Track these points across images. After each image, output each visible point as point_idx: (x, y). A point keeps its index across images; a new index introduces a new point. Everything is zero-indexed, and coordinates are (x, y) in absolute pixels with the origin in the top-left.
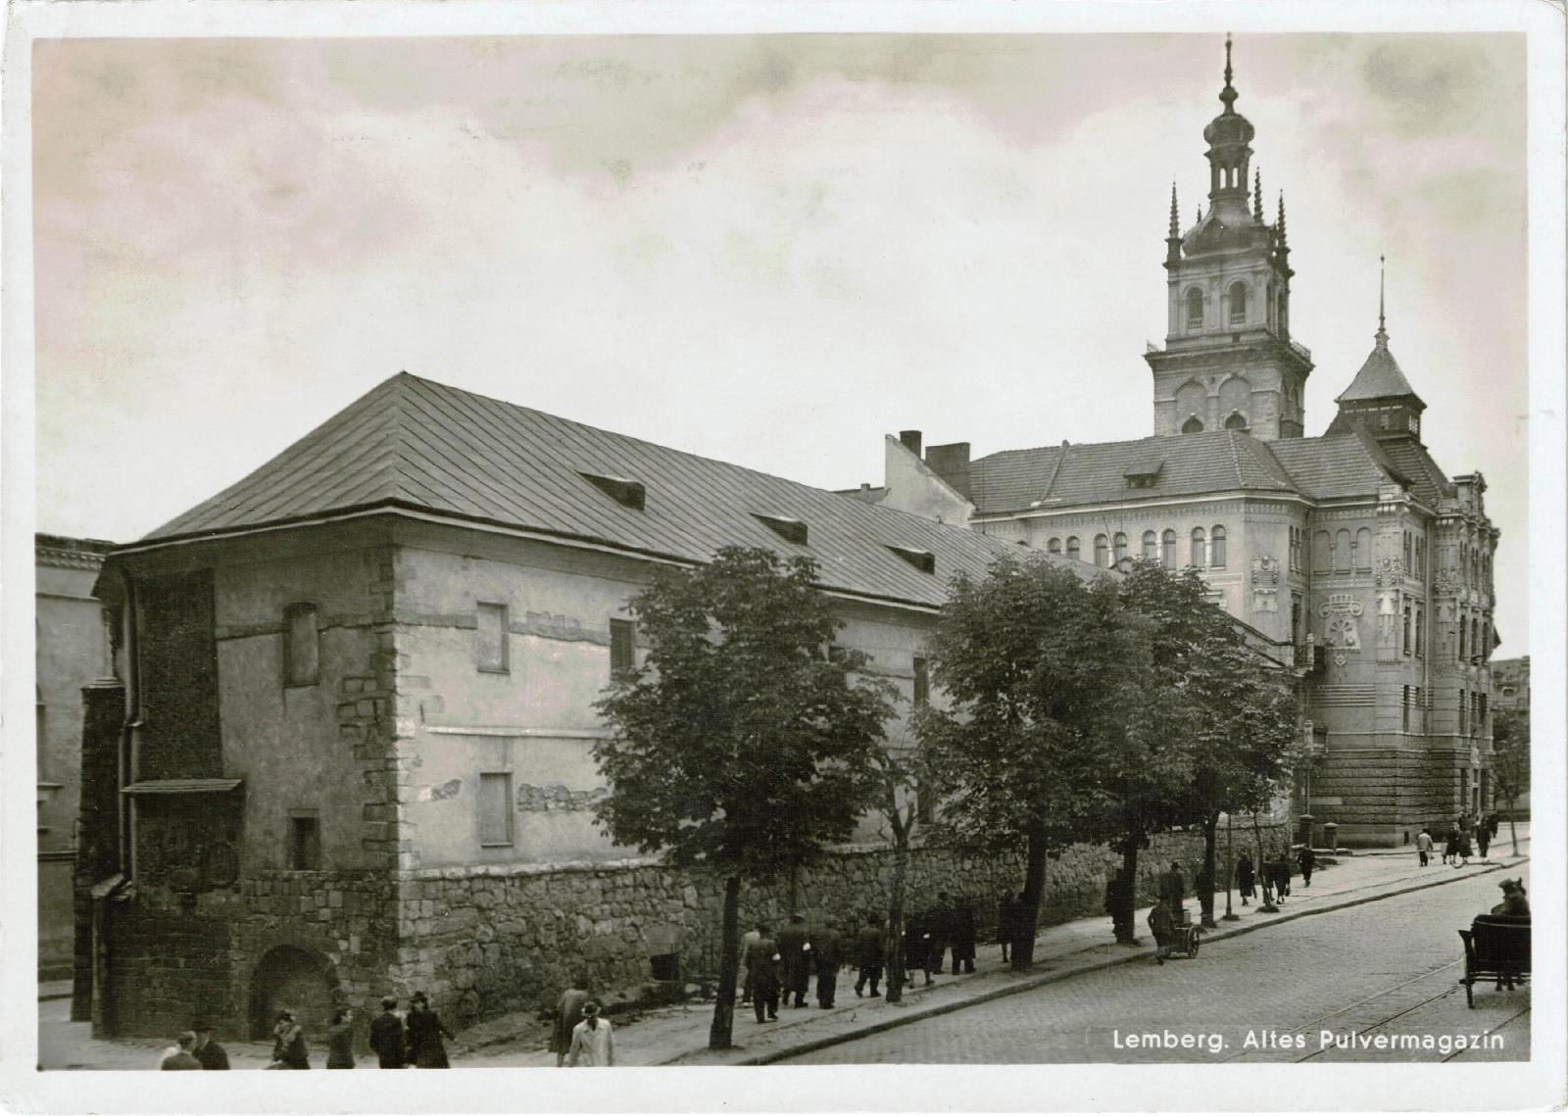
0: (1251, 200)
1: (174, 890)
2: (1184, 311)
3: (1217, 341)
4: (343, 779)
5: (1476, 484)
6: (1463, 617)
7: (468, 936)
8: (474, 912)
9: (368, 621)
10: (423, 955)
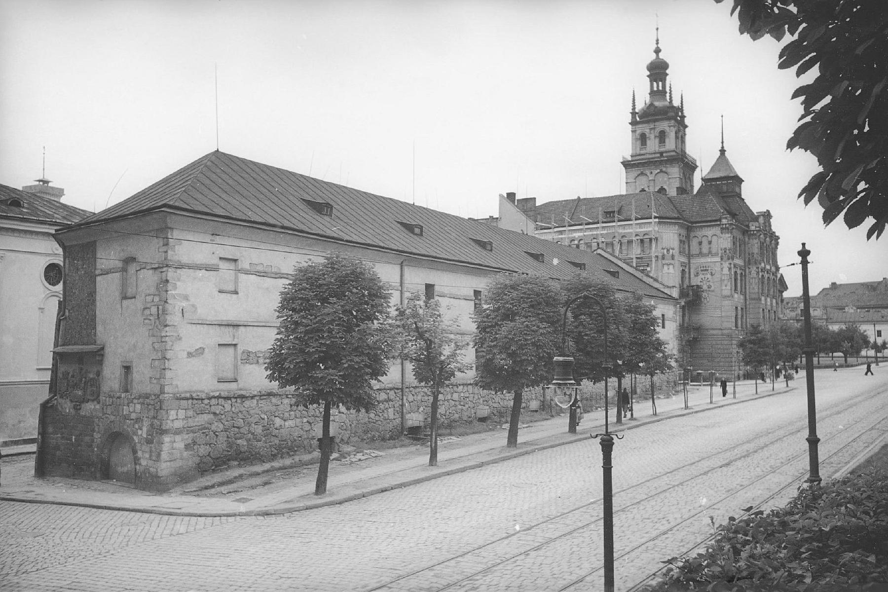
0: (668, 95)
1: (71, 401)
2: (639, 143)
3: (653, 156)
4: (143, 346)
5: (767, 215)
6: (736, 272)
7: (205, 428)
8: (212, 416)
9: (157, 266)
10: (178, 438)
